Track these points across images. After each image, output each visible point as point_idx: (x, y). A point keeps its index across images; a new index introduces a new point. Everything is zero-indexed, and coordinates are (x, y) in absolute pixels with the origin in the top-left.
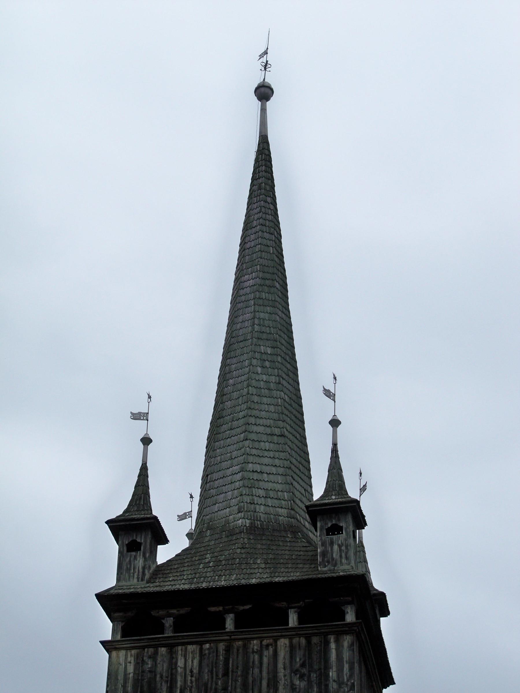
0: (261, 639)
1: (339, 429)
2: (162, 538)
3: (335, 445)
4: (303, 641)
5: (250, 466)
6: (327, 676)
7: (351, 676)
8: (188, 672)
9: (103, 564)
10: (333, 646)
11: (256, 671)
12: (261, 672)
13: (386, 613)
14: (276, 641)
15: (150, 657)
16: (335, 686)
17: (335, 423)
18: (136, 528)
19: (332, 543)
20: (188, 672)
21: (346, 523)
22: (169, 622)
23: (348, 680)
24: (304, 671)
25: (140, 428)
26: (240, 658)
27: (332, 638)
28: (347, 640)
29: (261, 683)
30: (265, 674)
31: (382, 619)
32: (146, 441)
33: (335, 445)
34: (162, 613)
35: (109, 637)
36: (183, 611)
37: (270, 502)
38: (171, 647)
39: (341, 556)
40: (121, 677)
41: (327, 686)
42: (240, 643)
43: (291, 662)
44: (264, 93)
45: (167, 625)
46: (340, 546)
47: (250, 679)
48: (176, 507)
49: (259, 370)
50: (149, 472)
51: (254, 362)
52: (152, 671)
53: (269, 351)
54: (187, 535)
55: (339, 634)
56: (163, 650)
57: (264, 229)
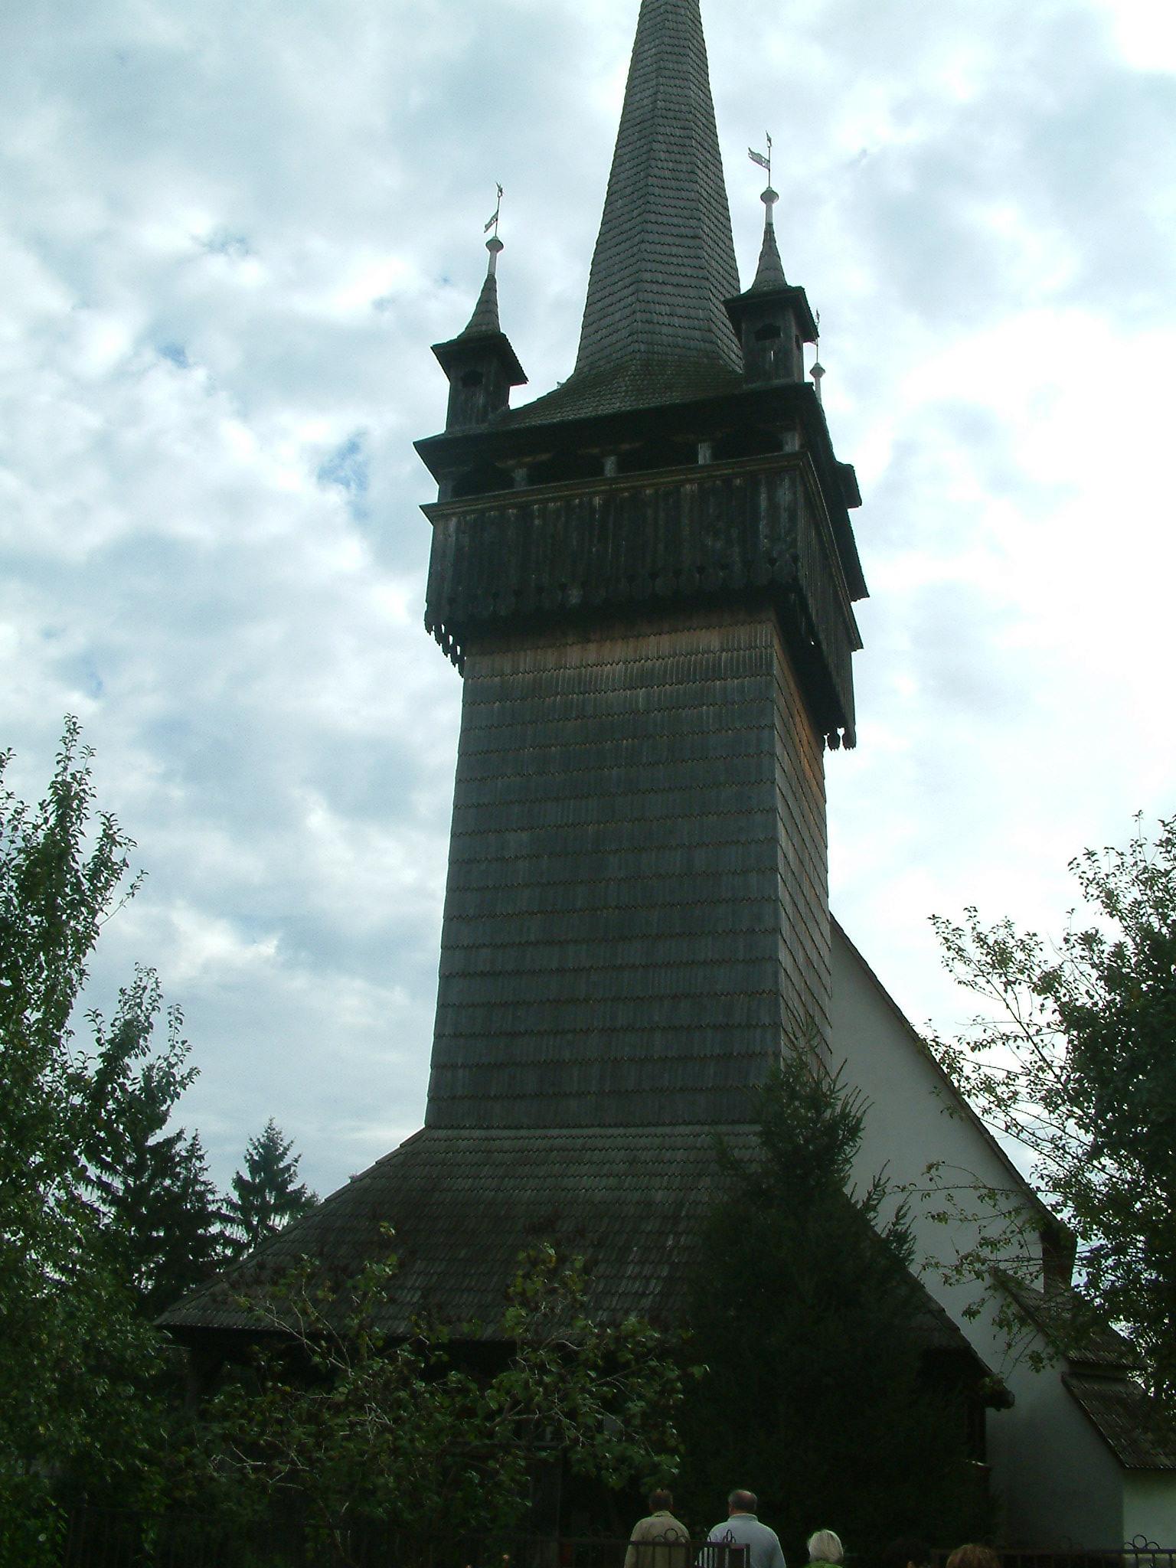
3: (769, 226)
5: (648, 276)
9: (428, 400)
13: (856, 502)
17: (769, 197)
18: (478, 358)
33: (769, 226)
34: (511, 462)
48: (547, 359)
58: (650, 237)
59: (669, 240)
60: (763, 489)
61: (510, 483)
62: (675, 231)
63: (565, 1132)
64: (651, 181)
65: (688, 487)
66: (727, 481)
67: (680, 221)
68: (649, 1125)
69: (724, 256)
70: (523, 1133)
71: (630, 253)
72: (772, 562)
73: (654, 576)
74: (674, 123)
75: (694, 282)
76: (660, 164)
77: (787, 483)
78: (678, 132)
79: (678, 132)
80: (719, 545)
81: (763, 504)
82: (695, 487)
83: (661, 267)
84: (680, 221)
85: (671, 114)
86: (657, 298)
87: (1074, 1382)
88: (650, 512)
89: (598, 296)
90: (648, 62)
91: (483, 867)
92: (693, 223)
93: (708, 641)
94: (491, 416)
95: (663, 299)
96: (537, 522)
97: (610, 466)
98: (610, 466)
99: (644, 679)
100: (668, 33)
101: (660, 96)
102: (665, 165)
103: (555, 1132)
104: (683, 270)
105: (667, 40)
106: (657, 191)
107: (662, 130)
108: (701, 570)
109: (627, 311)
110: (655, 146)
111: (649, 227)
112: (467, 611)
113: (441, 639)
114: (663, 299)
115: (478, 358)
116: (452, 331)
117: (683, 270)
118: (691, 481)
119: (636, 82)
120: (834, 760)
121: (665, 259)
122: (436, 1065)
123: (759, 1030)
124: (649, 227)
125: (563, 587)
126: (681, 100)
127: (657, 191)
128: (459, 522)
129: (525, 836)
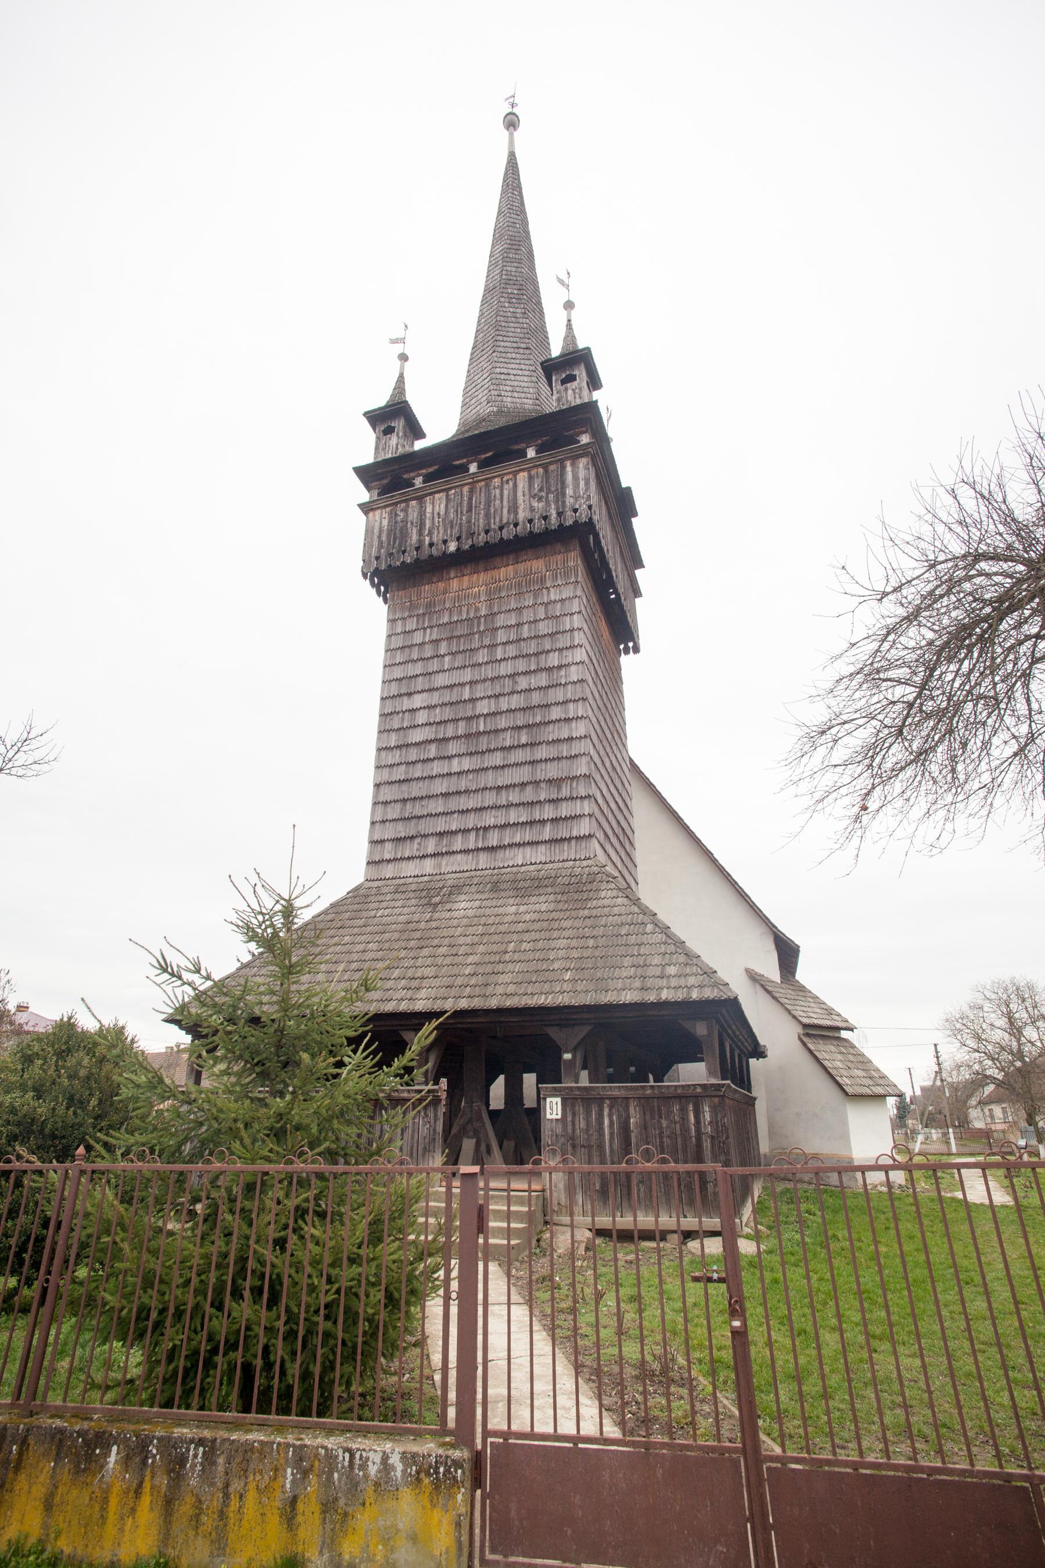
0: (502, 476)
1: (574, 313)
4: (541, 470)
5: (498, 370)
6: (564, 494)
7: (587, 489)
8: (436, 515)
9: (365, 447)
10: (569, 469)
11: (498, 502)
12: (502, 502)
14: (515, 476)
15: (402, 510)
16: (572, 500)
17: (569, 305)
19: (566, 389)
20: (436, 515)
24: (543, 494)
25: (399, 349)
26: (483, 495)
27: (568, 463)
28: (582, 462)
30: (505, 503)
31: (637, 572)
32: (404, 358)
34: (412, 475)
35: (368, 457)
36: (430, 470)
37: (516, 395)
38: (420, 499)
40: (376, 531)
41: (564, 502)
42: (483, 483)
43: (530, 490)
44: (511, 123)
46: (573, 390)
47: (492, 510)
49: (507, 305)
51: (502, 300)
52: (405, 521)
53: (516, 292)
55: (574, 458)
56: (414, 503)
72: (575, 511)
73: (501, 528)
87: (806, 1039)
95: (508, 383)
106: (503, 324)
108: (530, 521)
115: (393, 416)
124: (498, 343)
125: (445, 542)
127: (503, 324)
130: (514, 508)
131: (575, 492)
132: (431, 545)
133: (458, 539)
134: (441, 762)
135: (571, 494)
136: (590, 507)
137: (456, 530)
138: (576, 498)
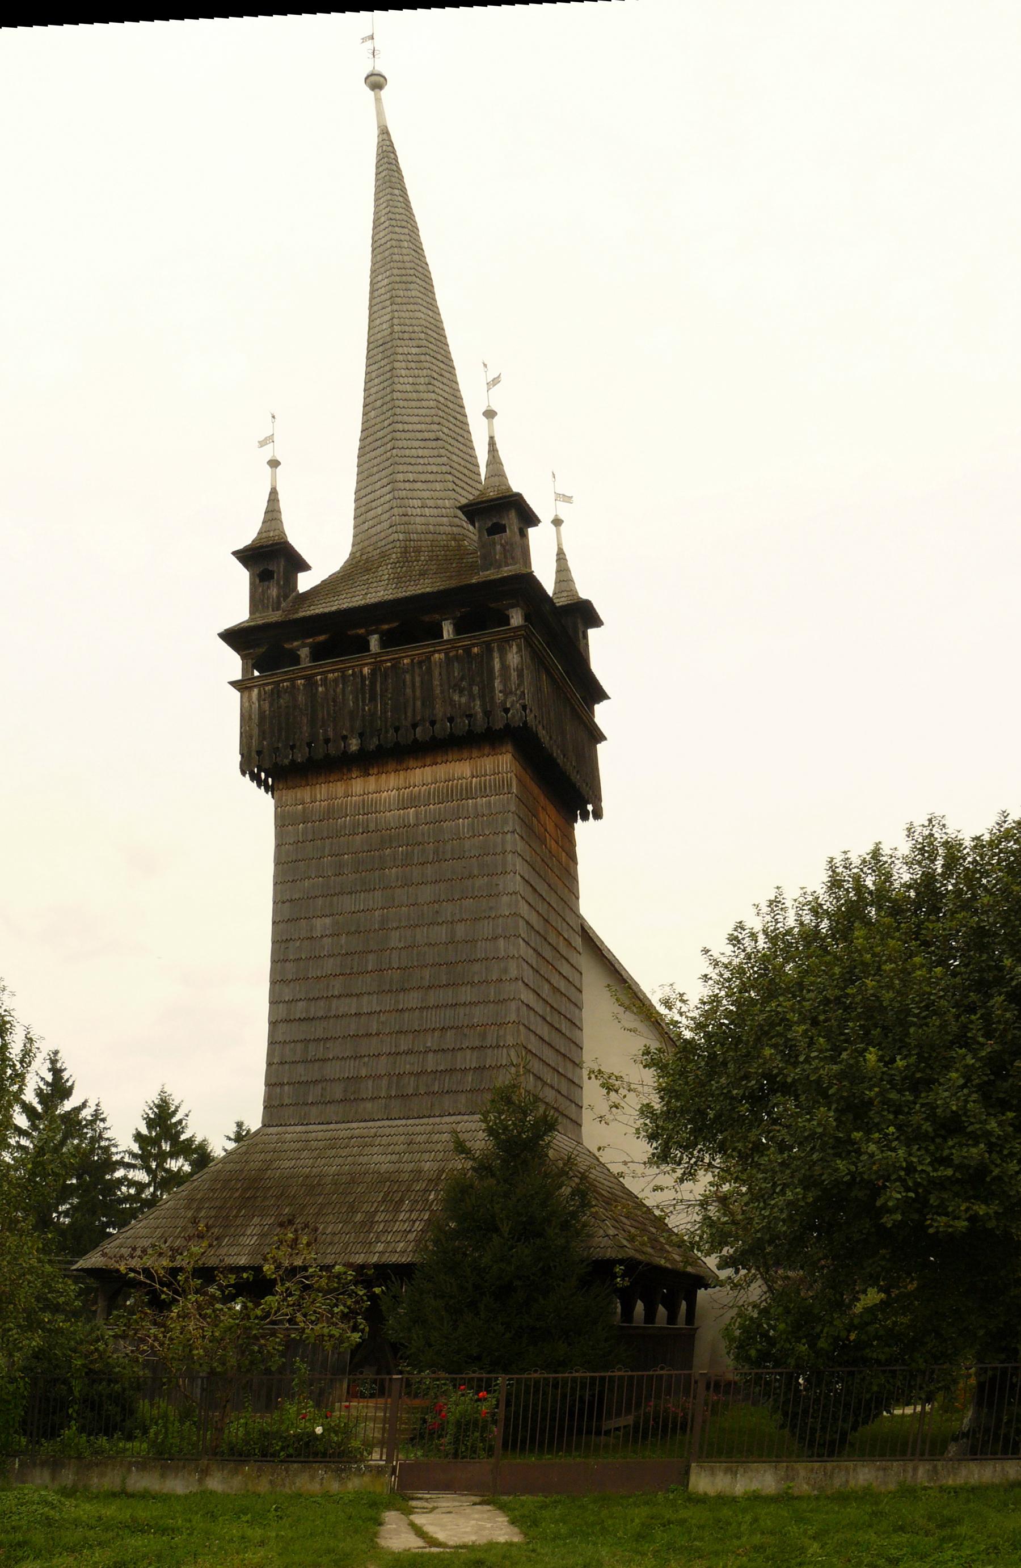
2: (302, 566)
5: (400, 477)
9: (234, 600)
12: (414, 691)
17: (490, 414)
18: (270, 559)
19: (494, 544)
21: (512, 520)
22: (304, 652)
23: (516, 690)
29: (414, 704)
34: (296, 644)
35: (238, 676)
39: (505, 557)
41: (492, 698)
42: (389, 664)
45: (303, 656)
50: (280, 497)
54: (563, 521)
57: (394, 223)
58: (400, 444)
59: (417, 444)
60: (496, 655)
61: (296, 660)
62: (419, 436)
63: (362, 1124)
64: (396, 395)
65: (437, 655)
66: (467, 650)
67: (423, 427)
68: (424, 1117)
69: (464, 448)
70: (332, 1126)
71: (384, 457)
72: (506, 711)
73: (414, 726)
74: (411, 343)
75: (439, 477)
76: (402, 380)
77: (515, 649)
78: (414, 351)
79: (414, 351)
80: (463, 700)
81: (497, 666)
82: (442, 656)
83: (410, 468)
84: (423, 427)
85: (406, 336)
86: (410, 494)
88: (408, 677)
89: (363, 492)
90: (383, 291)
91: (298, 944)
92: (435, 427)
93: (461, 769)
94: (283, 605)
95: (415, 494)
96: (320, 689)
97: (374, 641)
98: (374, 641)
99: (413, 801)
100: (395, 265)
101: (396, 321)
102: (406, 380)
103: (354, 1125)
104: (429, 468)
105: (395, 272)
106: (401, 403)
107: (400, 350)
109: (387, 507)
110: (397, 365)
111: (398, 435)
112: (275, 755)
113: (255, 777)
114: (415, 494)
115: (270, 559)
116: (247, 536)
117: (429, 468)
118: (439, 651)
119: (375, 308)
120: (582, 829)
121: (413, 461)
122: (268, 1084)
123: (505, 1050)
124: (398, 435)
125: (345, 738)
126: (414, 322)
127: (401, 403)
128: (259, 692)
129: (328, 921)
130: (428, 699)
131: (505, 686)
132: (327, 741)
133: (361, 735)
134: (348, 1000)
135: (501, 687)
136: (524, 707)
137: (358, 724)
138: (507, 693)
